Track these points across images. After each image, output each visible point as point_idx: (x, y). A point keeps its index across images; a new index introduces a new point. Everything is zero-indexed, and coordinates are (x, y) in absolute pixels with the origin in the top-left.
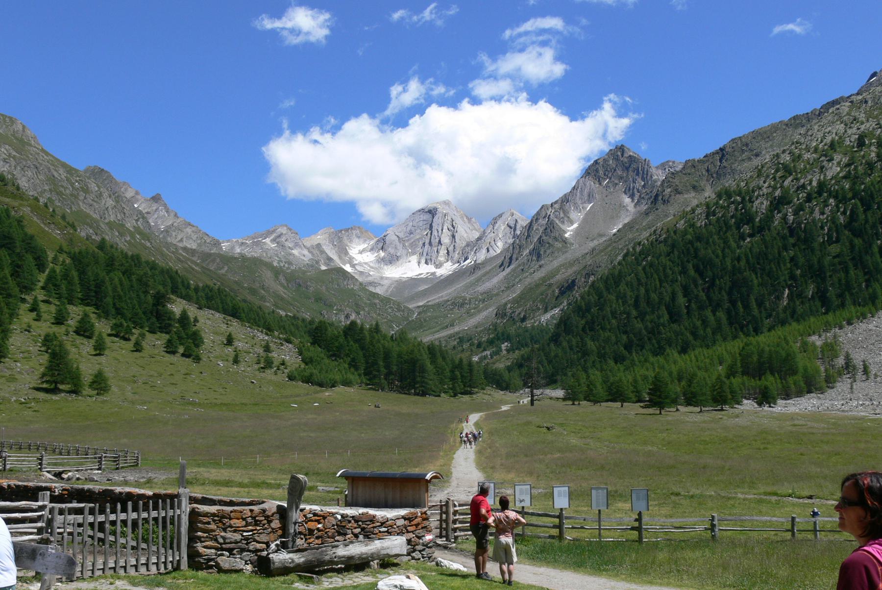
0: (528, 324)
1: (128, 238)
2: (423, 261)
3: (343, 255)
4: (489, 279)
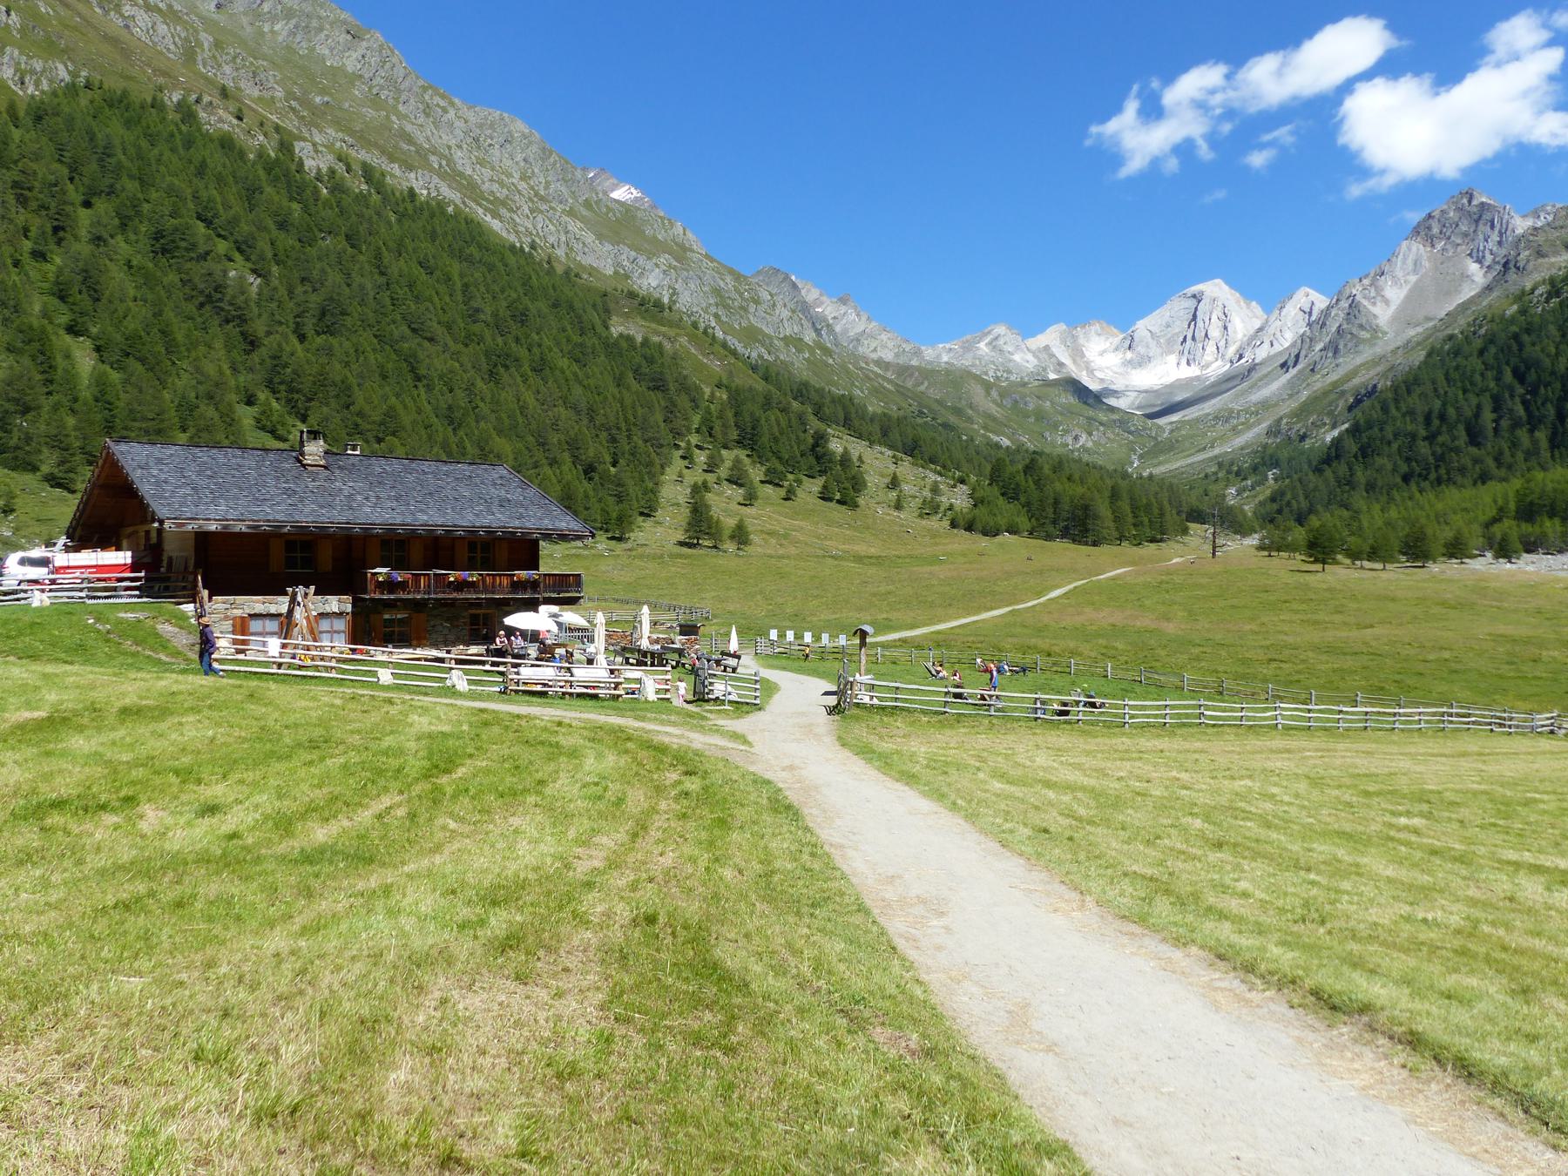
0: (1307, 444)
1: (807, 355)
2: (1184, 361)
3: (1078, 359)
4: (1267, 384)
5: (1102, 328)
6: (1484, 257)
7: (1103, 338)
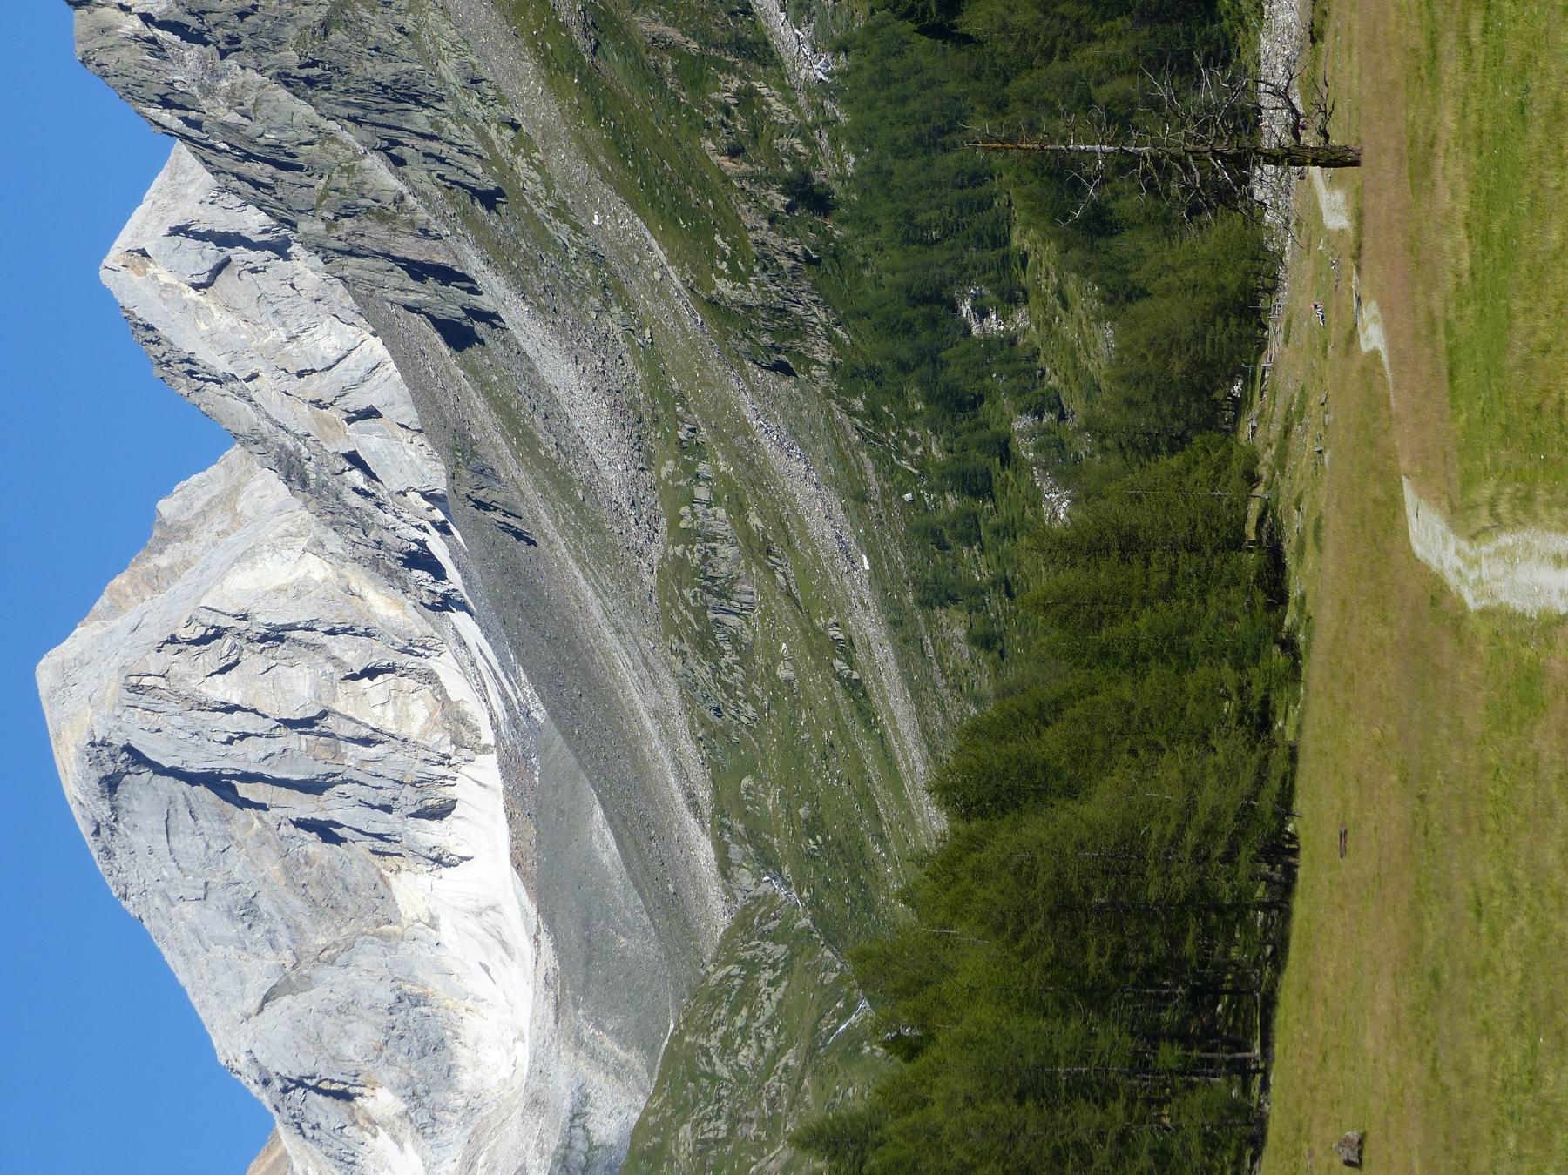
2: (432, 834)
4: (552, 412)
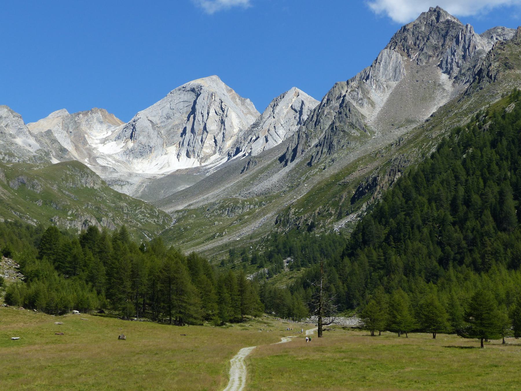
2: (184, 153)
4: (268, 176)
5: (104, 116)
6: (452, 68)
7: (105, 126)
